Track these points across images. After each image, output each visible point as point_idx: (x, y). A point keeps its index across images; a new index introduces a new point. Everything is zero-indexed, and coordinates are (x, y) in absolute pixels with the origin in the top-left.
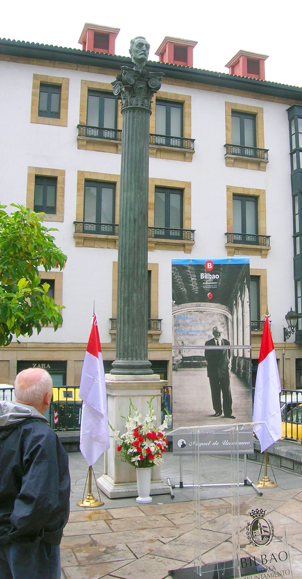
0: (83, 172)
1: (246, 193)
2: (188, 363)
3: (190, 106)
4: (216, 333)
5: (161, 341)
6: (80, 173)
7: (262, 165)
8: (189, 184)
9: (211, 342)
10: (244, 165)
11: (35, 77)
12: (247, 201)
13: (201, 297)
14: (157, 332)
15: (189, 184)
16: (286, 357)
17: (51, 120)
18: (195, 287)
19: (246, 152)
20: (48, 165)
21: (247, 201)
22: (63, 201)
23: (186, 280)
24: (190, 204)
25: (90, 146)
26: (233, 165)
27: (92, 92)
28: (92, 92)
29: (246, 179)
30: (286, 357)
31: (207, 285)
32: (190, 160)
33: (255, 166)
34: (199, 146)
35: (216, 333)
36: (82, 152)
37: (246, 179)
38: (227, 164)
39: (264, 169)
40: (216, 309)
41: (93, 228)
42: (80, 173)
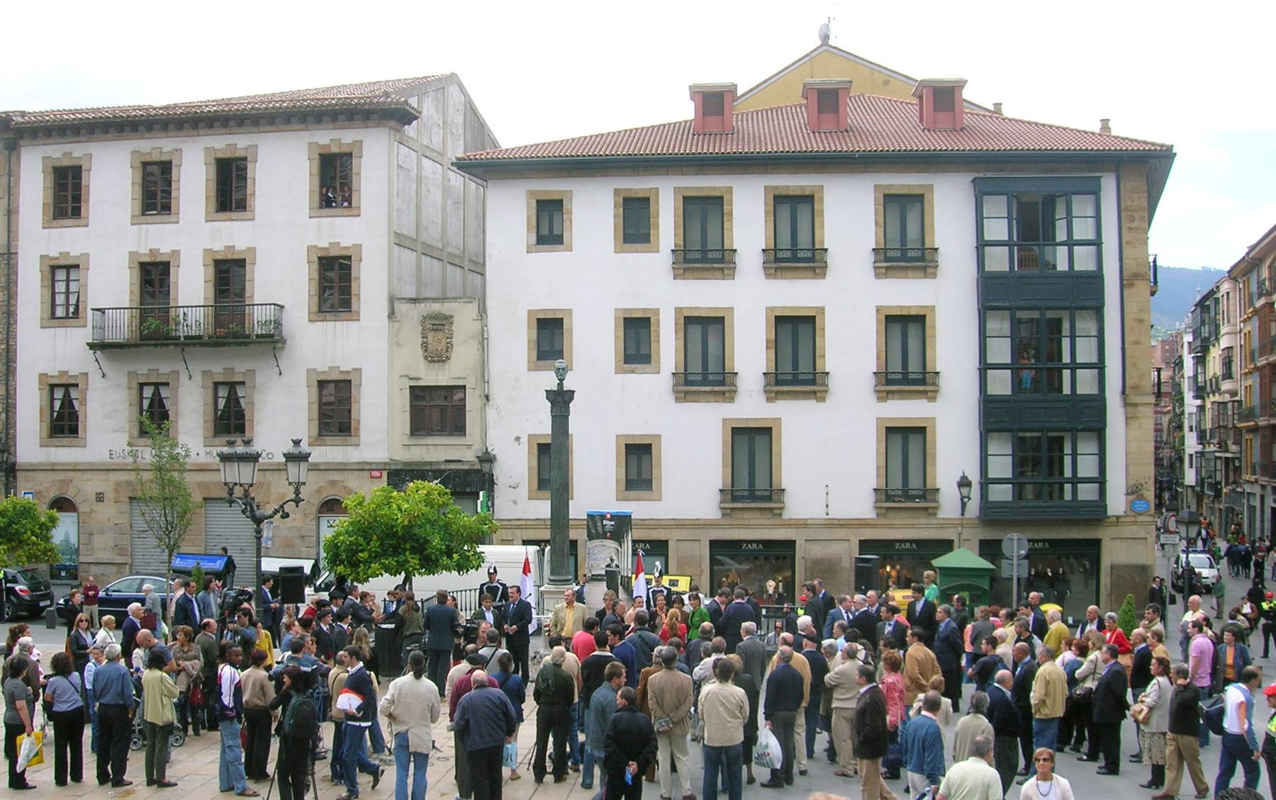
0: (681, 309)
1: (905, 313)
2: (595, 578)
3: (822, 199)
4: (612, 560)
5: (786, 515)
6: (678, 310)
7: (929, 271)
8: (822, 310)
9: (608, 566)
10: (903, 273)
11: (617, 192)
12: (905, 328)
13: (603, 536)
14: (779, 505)
15: (822, 310)
16: (964, 536)
17: (639, 246)
18: (601, 531)
19: (905, 253)
20: (637, 303)
21: (905, 328)
22: (658, 347)
23: (595, 526)
24: (824, 336)
25: (689, 274)
26: (886, 276)
27: (688, 201)
28: (688, 201)
29: (906, 293)
30: (964, 536)
31: (608, 528)
32: (823, 275)
33: (920, 273)
34: (834, 259)
35: (612, 560)
36: (680, 282)
37: (906, 293)
38: (877, 276)
39: (934, 276)
40: (612, 544)
41: (699, 378)
42: (678, 310)
